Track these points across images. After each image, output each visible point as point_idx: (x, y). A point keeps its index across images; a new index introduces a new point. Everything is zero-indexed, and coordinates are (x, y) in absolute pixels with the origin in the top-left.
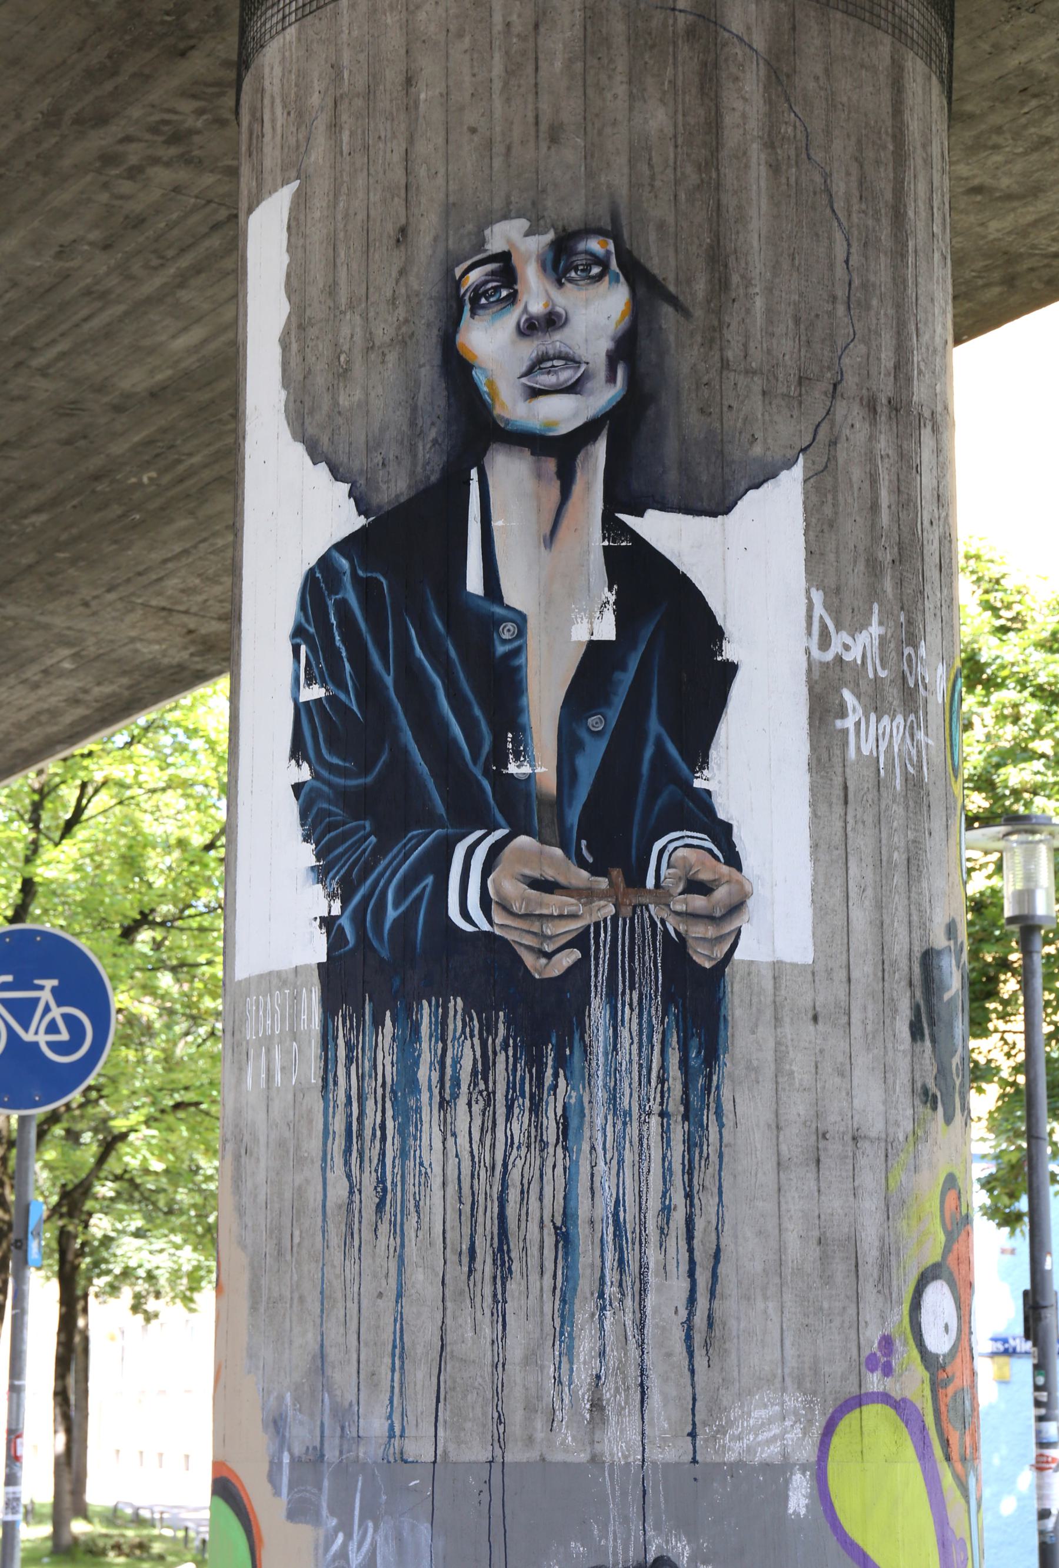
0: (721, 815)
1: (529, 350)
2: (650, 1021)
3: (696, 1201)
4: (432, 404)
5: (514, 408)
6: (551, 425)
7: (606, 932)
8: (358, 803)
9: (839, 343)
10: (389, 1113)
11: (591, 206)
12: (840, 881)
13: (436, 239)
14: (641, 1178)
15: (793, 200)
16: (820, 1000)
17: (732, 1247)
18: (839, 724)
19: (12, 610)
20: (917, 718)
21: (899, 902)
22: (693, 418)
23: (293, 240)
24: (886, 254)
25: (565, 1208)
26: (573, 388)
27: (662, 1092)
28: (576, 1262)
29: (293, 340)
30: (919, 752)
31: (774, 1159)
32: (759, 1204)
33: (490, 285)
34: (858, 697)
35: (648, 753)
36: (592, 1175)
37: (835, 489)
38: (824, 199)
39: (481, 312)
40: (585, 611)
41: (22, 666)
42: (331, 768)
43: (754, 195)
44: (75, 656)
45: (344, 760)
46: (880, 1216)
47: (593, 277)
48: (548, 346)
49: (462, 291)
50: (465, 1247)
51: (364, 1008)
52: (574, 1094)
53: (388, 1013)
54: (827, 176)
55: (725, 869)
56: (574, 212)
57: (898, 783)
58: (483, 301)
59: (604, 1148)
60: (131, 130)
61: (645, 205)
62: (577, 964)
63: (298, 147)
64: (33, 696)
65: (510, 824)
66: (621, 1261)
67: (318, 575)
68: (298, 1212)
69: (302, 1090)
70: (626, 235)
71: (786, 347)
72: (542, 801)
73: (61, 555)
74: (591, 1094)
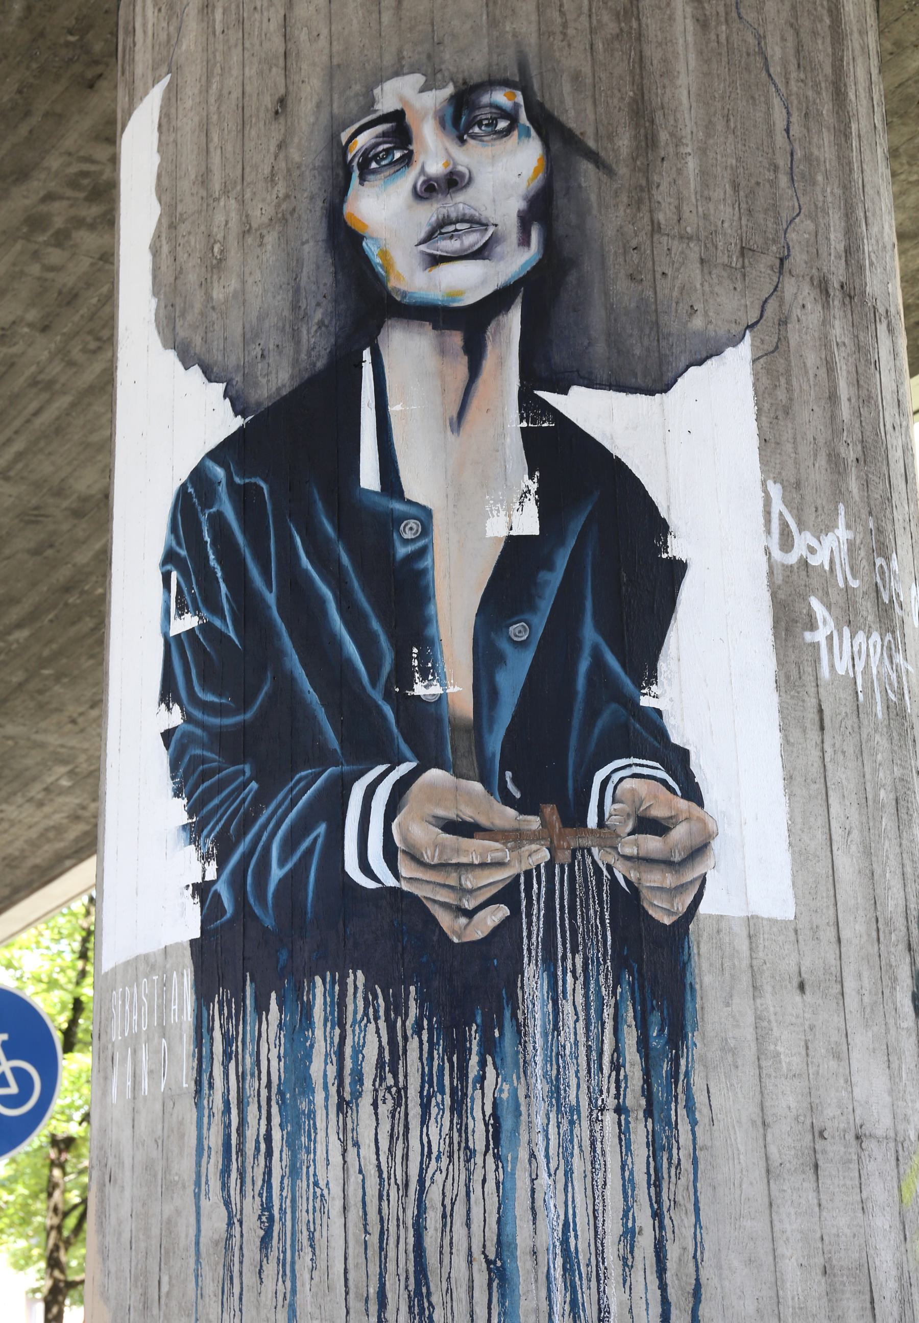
0: (675, 739)
1: (428, 214)
2: (598, 992)
3: (667, 1221)
4: (317, 283)
5: (410, 278)
6: (455, 295)
7: (539, 883)
8: (234, 745)
9: (784, 215)
10: (276, 1120)
11: (495, 56)
12: (821, 821)
13: (318, 105)
14: (596, 1192)
15: (725, 59)
16: (806, 964)
17: (715, 1281)
18: (808, 636)
19: (10, 729)
20: (894, 638)
21: (889, 847)
22: (621, 286)
23: (163, 138)
24: (829, 129)
25: (499, 1235)
26: (480, 253)
27: (617, 1081)
28: (515, 1306)
29: (164, 242)
30: (899, 677)
31: (762, 1164)
32: (747, 1223)
33: (381, 148)
34: (829, 607)
35: (584, 665)
36: (533, 1191)
37: (788, 373)
38: (760, 63)
39: (371, 177)
40: (501, 502)
41: (26, 785)
42: (205, 707)
43: (680, 48)
44: (71, 773)
45: (220, 696)
46: (895, 1236)
47: (500, 132)
48: (450, 212)
49: (350, 157)
50: (373, 1291)
51: (244, 991)
52: (506, 1087)
53: (273, 995)
54: (760, 38)
55: (683, 804)
56: (476, 62)
57: (879, 709)
58: (374, 165)
59: (547, 1156)
60: (52, 185)
61: (557, 54)
62: (504, 924)
63: (169, 41)
64: (39, 815)
65: (418, 756)
66: (574, 1304)
67: (190, 490)
68: (167, 1253)
69: (172, 1097)
70: (536, 86)
71: (725, 214)
72: (456, 726)
73: (46, 672)
74: (528, 1085)
